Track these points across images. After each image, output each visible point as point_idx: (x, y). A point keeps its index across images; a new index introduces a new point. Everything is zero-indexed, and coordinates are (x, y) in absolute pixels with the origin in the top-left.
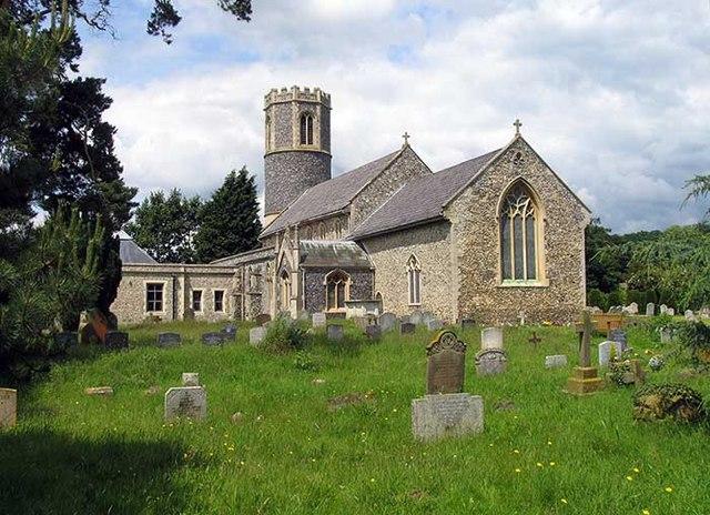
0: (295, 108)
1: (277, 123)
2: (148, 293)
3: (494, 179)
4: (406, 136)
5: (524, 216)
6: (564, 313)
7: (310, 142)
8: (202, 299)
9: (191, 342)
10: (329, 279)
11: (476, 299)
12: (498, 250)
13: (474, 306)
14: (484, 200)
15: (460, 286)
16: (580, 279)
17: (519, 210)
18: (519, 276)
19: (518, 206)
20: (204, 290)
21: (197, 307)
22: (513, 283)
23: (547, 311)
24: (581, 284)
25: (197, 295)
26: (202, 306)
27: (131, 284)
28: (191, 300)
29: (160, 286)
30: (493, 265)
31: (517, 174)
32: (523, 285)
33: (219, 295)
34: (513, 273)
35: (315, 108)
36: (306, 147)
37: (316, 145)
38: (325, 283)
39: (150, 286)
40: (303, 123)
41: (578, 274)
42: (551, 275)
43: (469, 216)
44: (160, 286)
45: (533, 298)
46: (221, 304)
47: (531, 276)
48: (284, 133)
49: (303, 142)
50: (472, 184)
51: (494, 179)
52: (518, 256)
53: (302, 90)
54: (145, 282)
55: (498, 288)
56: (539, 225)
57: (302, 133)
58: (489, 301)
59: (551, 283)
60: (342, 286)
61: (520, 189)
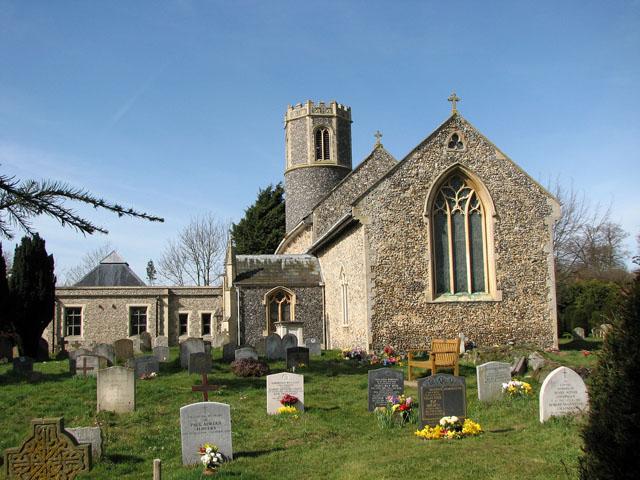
0: (309, 121)
1: (293, 140)
2: (79, 323)
5: (466, 212)
7: (327, 156)
8: (189, 322)
9: (93, 368)
10: (270, 297)
11: (399, 319)
12: (427, 256)
13: (395, 327)
14: (408, 193)
15: (374, 303)
17: (458, 206)
19: (457, 200)
20: (190, 313)
21: (183, 330)
23: (500, 332)
25: (184, 318)
26: (189, 330)
27: (114, 307)
28: (62, 324)
29: (144, 309)
30: (420, 274)
31: (453, 160)
32: (463, 299)
33: (206, 318)
35: (330, 122)
36: (323, 162)
37: (333, 159)
38: (264, 302)
39: (133, 310)
41: (544, 283)
42: (504, 286)
43: (385, 215)
44: (144, 309)
45: (478, 317)
46: (79, 328)
49: (318, 156)
50: (389, 175)
51: (423, 168)
54: (128, 306)
56: (488, 223)
58: (416, 320)
60: (286, 305)
61: (455, 178)
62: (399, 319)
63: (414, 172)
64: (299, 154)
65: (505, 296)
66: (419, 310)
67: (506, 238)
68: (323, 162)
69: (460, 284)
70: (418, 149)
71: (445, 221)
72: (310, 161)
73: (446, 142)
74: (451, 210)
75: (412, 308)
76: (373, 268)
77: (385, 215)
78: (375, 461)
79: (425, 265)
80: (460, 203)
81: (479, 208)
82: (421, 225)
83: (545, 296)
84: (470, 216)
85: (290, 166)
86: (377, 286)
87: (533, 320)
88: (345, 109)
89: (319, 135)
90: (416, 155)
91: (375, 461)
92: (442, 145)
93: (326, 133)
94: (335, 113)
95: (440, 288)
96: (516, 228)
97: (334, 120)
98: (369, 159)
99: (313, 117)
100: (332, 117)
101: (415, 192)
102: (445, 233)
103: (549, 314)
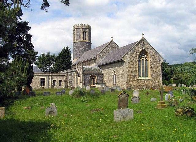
0: (81, 30)
1: (76, 34)
2: (41, 81)
3: (136, 49)
4: (112, 38)
5: (145, 59)
6: (156, 86)
7: (86, 39)
8: (56, 82)
9: (53, 94)
10: (91, 77)
11: (131, 83)
12: (137, 69)
13: (131, 84)
14: (134, 55)
15: (127, 79)
16: (160, 77)
17: (143, 58)
18: (143, 76)
19: (143, 57)
20: (56, 80)
21: (54, 85)
22: (142, 78)
23: (151, 86)
24: (160, 78)
25: (54, 81)
26: (56, 84)
27: (36, 78)
28: (53, 83)
29: (44, 79)
30: (136, 73)
31: (143, 48)
32: (144, 78)
33: (60, 81)
34: (142, 75)
35: (87, 30)
36: (84, 40)
37: (87, 40)
38: (90, 78)
39: (41, 79)
40: (84, 34)
41: (160, 76)
42: (152, 76)
43: (129, 59)
44: (44, 79)
45: (147, 82)
46: (61, 84)
47: (147, 76)
48: (78, 37)
49: (84, 39)
50: (130, 51)
51: (136, 49)
52: (143, 71)
53: (83, 25)
54: (40, 78)
55: (138, 79)
56: (149, 62)
57: (83, 37)
58: (135, 83)
60: (94, 79)
61: (144, 52)
65: (152, 78)
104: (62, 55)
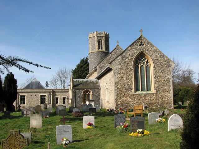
0: (96, 38)
1: (91, 44)
2: (25, 100)
5: (145, 66)
7: (102, 49)
8: (59, 100)
9: (29, 114)
10: (84, 92)
11: (124, 99)
12: (133, 79)
13: (123, 101)
14: (127, 60)
15: (116, 94)
17: (142, 64)
20: (59, 97)
21: (57, 103)
23: (155, 103)
25: (57, 99)
26: (59, 102)
27: (35, 95)
28: (19, 101)
29: (45, 96)
30: (131, 85)
31: (141, 50)
32: (144, 93)
33: (64, 99)
35: (103, 38)
36: (100, 50)
37: (104, 49)
38: (82, 94)
39: (41, 96)
41: (169, 88)
42: (157, 89)
43: (120, 67)
44: (45, 96)
45: (149, 98)
46: (25, 102)
49: (99, 49)
50: (121, 54)
51: (132, 52)
54: (40, 95)
56: (152, 69)
58: (129, 99)
59: (157, 92)
60: (89, 95)
61: (142, 55)
62: (124, 99)
63: (129, 53)
64: (93, 48)
66: (130, 96)
67: (157, 74)
68: (100, 50)
69: (143, 88)
70: (130, 46)
71: (138, 69)
72: (96, 50)
73: (139, 44)
74: (140, 65)
75: (128, 96)
76: (116, 83)
77: (120, 67)
78: (117, 143)
79: (132, 82)
80: (143, 63)
81: (149, 65)
82: (131, 70)
83: (170, 92)
84: (146, 67)
85: (90, 51)
86: (117, 89)
87: (166, 99)
88: (107, 34)
89: (99, 42)
90: (129, 48)
91: (117, 143)
92: (137, 45)
93: (101, 41)
94: (104, 35)
95: (137, 89)
96: (161, 71)
97: (104, 37)
98: (115, 49)
99: (97, 36)
100: (103, 36)
101: (129, 60)
102: (138, 72)
103: (171, 97)
104: (81, 67)
